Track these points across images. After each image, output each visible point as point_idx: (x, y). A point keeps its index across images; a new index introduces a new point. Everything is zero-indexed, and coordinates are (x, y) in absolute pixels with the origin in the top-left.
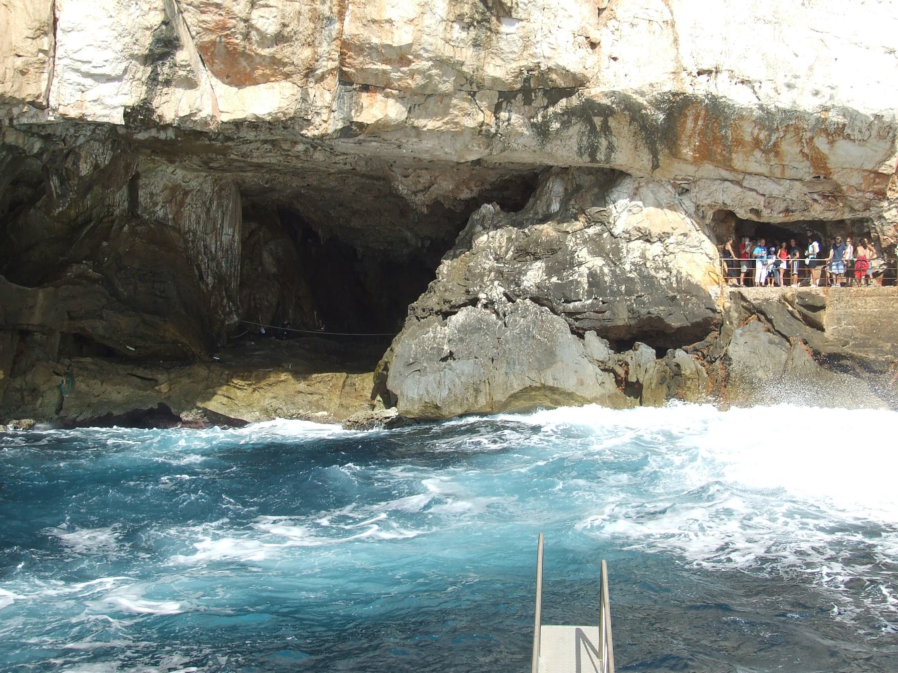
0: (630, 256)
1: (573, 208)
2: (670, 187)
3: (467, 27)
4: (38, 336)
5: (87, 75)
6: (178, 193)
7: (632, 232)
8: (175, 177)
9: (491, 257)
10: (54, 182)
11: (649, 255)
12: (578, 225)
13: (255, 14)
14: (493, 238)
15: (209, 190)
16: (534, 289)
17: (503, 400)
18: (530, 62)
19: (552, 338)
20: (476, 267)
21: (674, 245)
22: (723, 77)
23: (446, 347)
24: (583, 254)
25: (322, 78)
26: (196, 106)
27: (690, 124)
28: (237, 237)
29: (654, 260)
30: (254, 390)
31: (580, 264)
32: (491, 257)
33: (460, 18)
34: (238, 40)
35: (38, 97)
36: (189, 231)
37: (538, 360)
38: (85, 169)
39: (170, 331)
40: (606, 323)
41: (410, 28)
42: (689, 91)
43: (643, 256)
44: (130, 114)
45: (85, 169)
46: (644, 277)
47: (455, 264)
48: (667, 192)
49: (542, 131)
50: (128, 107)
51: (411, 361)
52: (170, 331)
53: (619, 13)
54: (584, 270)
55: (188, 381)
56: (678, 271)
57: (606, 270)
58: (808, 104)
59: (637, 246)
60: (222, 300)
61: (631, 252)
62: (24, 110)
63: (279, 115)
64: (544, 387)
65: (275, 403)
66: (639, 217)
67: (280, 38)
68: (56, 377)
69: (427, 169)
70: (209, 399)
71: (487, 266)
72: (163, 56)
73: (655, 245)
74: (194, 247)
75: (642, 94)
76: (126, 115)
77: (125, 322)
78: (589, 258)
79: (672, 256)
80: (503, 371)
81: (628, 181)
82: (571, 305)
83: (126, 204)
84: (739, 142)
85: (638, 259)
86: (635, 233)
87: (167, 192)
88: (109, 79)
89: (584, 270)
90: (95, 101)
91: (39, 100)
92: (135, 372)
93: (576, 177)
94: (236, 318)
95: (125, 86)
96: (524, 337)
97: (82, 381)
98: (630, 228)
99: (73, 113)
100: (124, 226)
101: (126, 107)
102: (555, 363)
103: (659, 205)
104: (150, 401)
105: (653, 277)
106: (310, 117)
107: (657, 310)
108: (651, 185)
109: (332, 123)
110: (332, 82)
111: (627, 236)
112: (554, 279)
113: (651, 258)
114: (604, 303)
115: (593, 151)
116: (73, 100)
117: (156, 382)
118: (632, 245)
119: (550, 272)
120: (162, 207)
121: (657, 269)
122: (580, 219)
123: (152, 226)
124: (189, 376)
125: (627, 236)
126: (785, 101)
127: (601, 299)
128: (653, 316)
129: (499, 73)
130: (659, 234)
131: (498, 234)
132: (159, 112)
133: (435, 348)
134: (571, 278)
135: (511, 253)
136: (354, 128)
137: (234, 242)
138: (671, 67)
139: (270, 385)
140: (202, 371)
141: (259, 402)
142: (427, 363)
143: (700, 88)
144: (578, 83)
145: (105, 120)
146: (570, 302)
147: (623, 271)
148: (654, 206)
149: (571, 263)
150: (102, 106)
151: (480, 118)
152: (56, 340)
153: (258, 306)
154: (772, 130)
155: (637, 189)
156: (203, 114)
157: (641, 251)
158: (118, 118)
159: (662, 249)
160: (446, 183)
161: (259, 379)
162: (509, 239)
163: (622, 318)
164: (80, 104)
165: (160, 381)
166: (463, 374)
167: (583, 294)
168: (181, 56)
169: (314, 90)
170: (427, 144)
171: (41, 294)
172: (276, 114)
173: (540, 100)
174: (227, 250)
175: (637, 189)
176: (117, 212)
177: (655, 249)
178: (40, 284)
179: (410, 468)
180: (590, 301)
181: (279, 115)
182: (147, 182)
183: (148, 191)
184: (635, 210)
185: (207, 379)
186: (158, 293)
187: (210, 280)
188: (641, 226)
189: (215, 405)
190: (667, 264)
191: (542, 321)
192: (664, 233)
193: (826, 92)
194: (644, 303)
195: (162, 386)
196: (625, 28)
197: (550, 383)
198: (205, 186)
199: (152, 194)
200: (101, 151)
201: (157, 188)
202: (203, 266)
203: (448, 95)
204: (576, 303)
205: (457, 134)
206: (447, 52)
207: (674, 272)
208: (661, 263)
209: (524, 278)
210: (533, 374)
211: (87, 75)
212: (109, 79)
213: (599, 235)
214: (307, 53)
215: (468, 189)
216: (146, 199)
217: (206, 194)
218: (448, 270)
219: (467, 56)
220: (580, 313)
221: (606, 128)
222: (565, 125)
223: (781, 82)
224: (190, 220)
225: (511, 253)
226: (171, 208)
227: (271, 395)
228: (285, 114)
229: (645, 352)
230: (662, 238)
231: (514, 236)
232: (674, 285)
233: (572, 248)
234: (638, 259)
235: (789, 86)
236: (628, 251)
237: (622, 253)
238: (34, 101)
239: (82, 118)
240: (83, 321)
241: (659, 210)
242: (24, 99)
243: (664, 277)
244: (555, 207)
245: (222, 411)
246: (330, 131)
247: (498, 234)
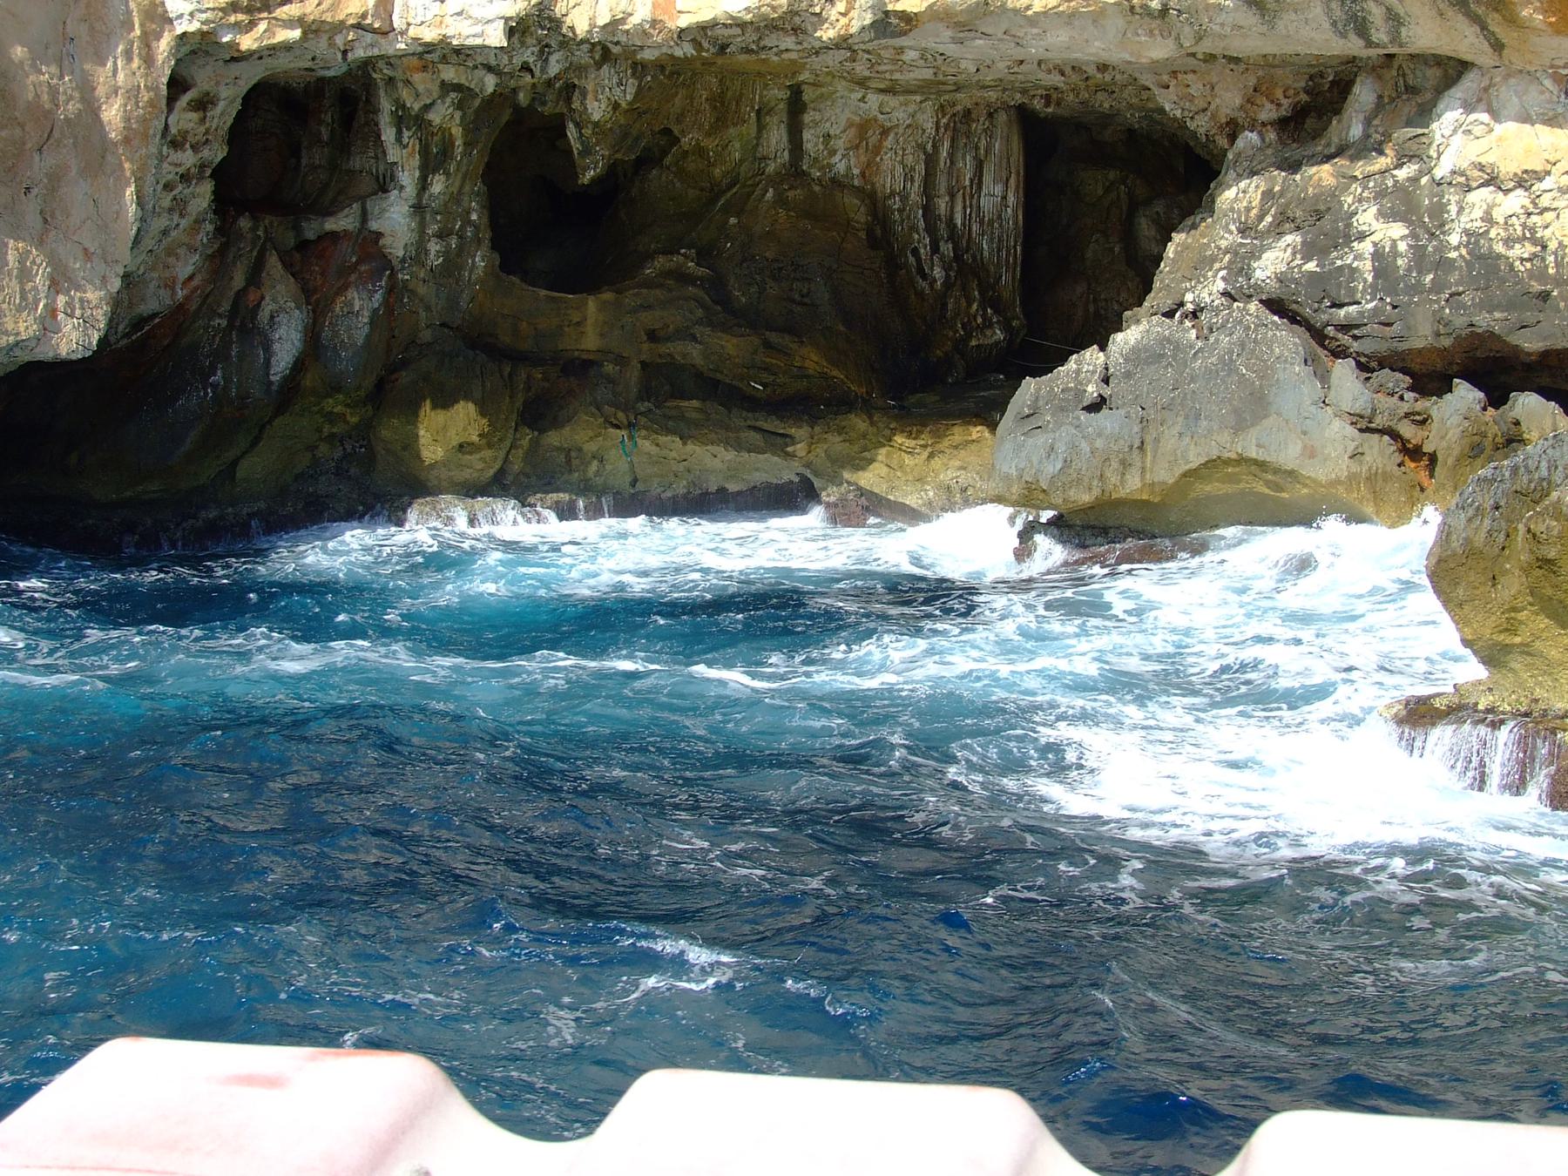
0: (1463, 219)
1: (1376, 132)
2: (1548, 83)
4: (609, 368)
6: (870, 133)
7: (1468, 173)
8: (867, 106)
9: (1233, 228)
11: (1498, 216)
12: (1382, 162)
14: (1244, 192)
15: (930, 125)
16: (1274, 284)
17: (1170, 482)
19: (1265, 372)
20: (1208, 245)
21: (1555, 194)
23: (1090, 388)
24: (1367, 218)
26: (622, 7)
28: (1011, 199)
29: (1506, 223)
30: (931, 456)
31: (1362, 237)
32: (1233, 228)
35: (364, 16)
36: (893, 194)
37: (1236, 411)
39: (812, 360)
40: (1395, 344)
43: (1488, 219)
44: (517, 29)
46: (1481, 257)
47: (1189, 241)
48: (1542, 93)
50: (511, 18)
51: (1027, 411)
52: (812, 360)
54: (1366, 247)
55: (838, 439)
56: (1560, 243)
57: (1402, 247)
60: (969, 305)
61: (1467, 211)
62: (350, 38)
63: (763, 9)
64: (1241, 460)
65: (964, 478)
66: (1483, 144)
68: (611, 430)
69: (1194, 72)
70: (863, 469)
71: (1223, 244)
73: (1512, 195)
74: (903, 221)
76: (511, 32)
77: (733, 346)
78: (1376, 225)
79: (1549, 216)
80: (1175, 431)
81: (1475, 70)
82: (1342, 312)
83: (786, 154)
85: (1479, 223)
86: (1476, 173)
87: (852, 132)
89: (1366, 247)
90: (459, 14)
91: (368, 21)
92: (760, 424)
93: (1408, 72)
94: (999, 335)
96: (1223, 370)
97: (645, 438)
98: (1465, 165)
99: (429, 35)
100: (767, 191)
101: (507, 19)
102: (1266, 416)
103: (1526, 119)
104: (782, 471)
105: (1499, 256)
106: (817, 9)
108: (1512, 81)
109: (856, 16)
111: (1462, 179)
112: (1311, 266)
113: (1501, 221)
114: (1395, 307)
116: (429, 16)
117: (791, 439)
118: (1472, 197)
119: (1308, 251)
120: (844, 156)
121: (1509, 242)
122: (1387, 151)
123: (817, 188)
124: (841, 430)
125: (1462, 179)
127: (1388, 300)
128: (1480, 331)
130: (1515, 174)
131: (1253, 185)
132: (568, 21)
133: (1071, 389)
134: (1339, 263)
135: (1269, 219)
136: (894, 21)
137: (1007, 206)
139: (956, 447)
140: (859, 423)
141: (937, 475)
142: (1053, 415)
145: (478, 41)
146: (1341, 306)
147: (1443, 247)
148: (1517, 121)
149: (1348, 236)
150: (470, 21)
152: (634, 374)
153: (1103, 312)
155: (1486, 90)
156: (634, 20)
157: (1485, 207)
158: (495, 37)
159: (1527, 202)
160: (1229, 94)
161: (938, 436)
162: (1268, 195)
163: (1421, 335)
165: (798, 439)
166: (1099, 435)
167: (1364, 289)
171: (592, 304)
172: (759, 8)
174: (991, 222)
175: (1486, 90)
176: (771, 168)
177: (1515, 202)
178: (592, 288)
179: (160, 591)
180: (1374, 303)
181: (763, 9)
182: (818, 117)
183: (820, 131)
184: (1478, 130)
185: (864, 436)
186: (797, 297)
187: (938, 273)
188: (1483, 160)
189: (871, 478)
190: (1533, 230)
191: (1255, 341)
192: (1526, 172)
194: (1464, 307)
195: (799, 446)
197: (1253, 453)
198: (920, 117)
199: (827, 137)
200: (615, 80)
201: (835, 126)
202: (922, 251)
204: (1352, 309)
207: (1553, 245)
208: (1519, 229)
209: (1255, 265)
210: (1225, 438)
213: (1414, 180)
215: (1272, 102)
216: (816, 144)
217: (924, 131)
218: (1176, 252)
220: (1357, 326)
224: (893, 176)
225: (1269, 219)
226: (858, 157)
227: (958, 463)
228: (774, 8)
229: (1465, 395)
230: (1524, 181)
231: (1277, 188)
232: (1551, 271)
233: (1350, 206)
234: (1479, 223)
236: (1461, 210)
237: (1448, 212)
238: (359, 24)
239: (444, 41)
240: (669, 344)
241: (1527, 127)
242: (342, 22)
243: (1526, 256)
244: (1356, 131)
245: (880, 489)
246: (853, 30)
247: (1253, 185)
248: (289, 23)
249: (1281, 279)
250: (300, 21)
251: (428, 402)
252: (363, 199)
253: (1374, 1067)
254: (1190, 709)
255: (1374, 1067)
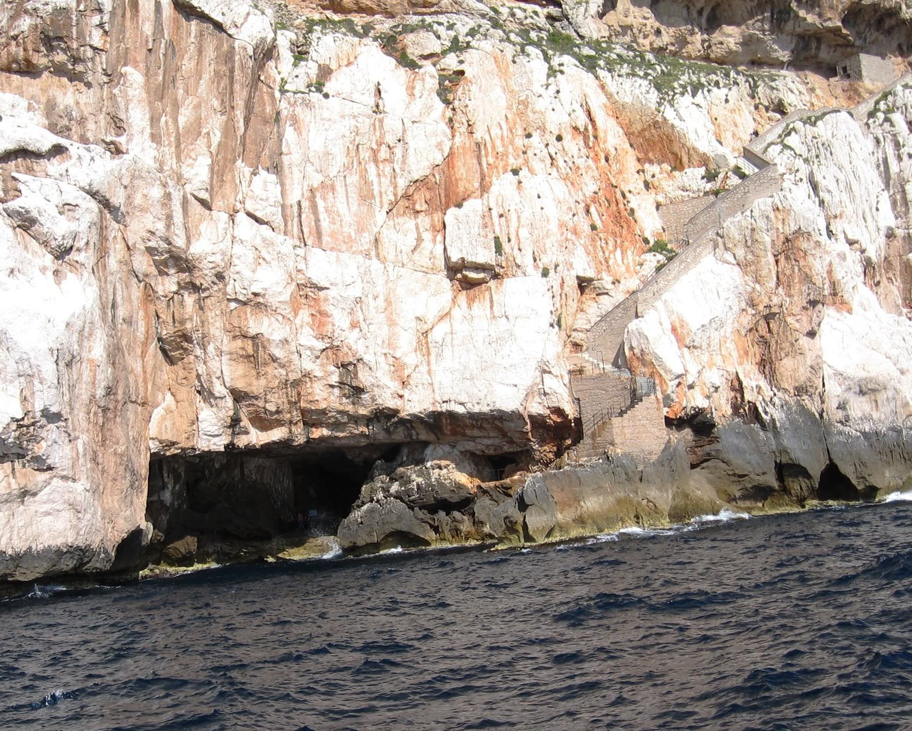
3: (348, 398)
5: (210, 435)
10: (207, 472)
13: (267, 405)
18: (376, 407)
22: (453, 402)
24: (414, 477)
25: (296, 423)
27: (444, 422)
33: (344, 395)
34: (262, 415)
38: (217, 466)
41: (325, 402)
42: (439, 410)
44: (226, 447)
45: (217, 466)
49: (387, 431)
53: (411, 382)
54: (415, 483)
58: (485, 409)
59: (437, 471)
67: (278, 412)
72: (235, 425)
75: (421, 413)
84: (467, 426)
88: (218, 436)
89: (415, 483)
95: (223, 437)
99: (206, 449)
107: (446, 496)
110: (301, 424)
115: (411, 436)
119: (401, 485)
121: (445, 480)
126: (476, 409)
129: (364, 413)
138: (432, 401)
143: (445, 408)
144: (396, 412)
149: (410, 481)
151: (361, 429)
154: (477, 421)
158: (222, 449)
164: (208, 446)
168: (242, 424)
169: (293, 429)
170: (343, 442)
173: (383, 420)
193: (492, 404)
196: (414, 388)
203: (345, 423)
205: (354, 436)
206: (342, 408)
211: (210, 435)
212: (218, 436)
214: (289, 415)
219: (350, 408)
221: (413, 427)
222: (396, 428)
223: (475, 402)
229: (442, 514)
235: (478, 403)
244: (405, 458)
248: (177, 449)
249: (397, 492)
250: (181, 448)
251: (143, 544)
252: (158, 492)
253: (791, 665)
254: (143, 608)
255: (791, 665)
